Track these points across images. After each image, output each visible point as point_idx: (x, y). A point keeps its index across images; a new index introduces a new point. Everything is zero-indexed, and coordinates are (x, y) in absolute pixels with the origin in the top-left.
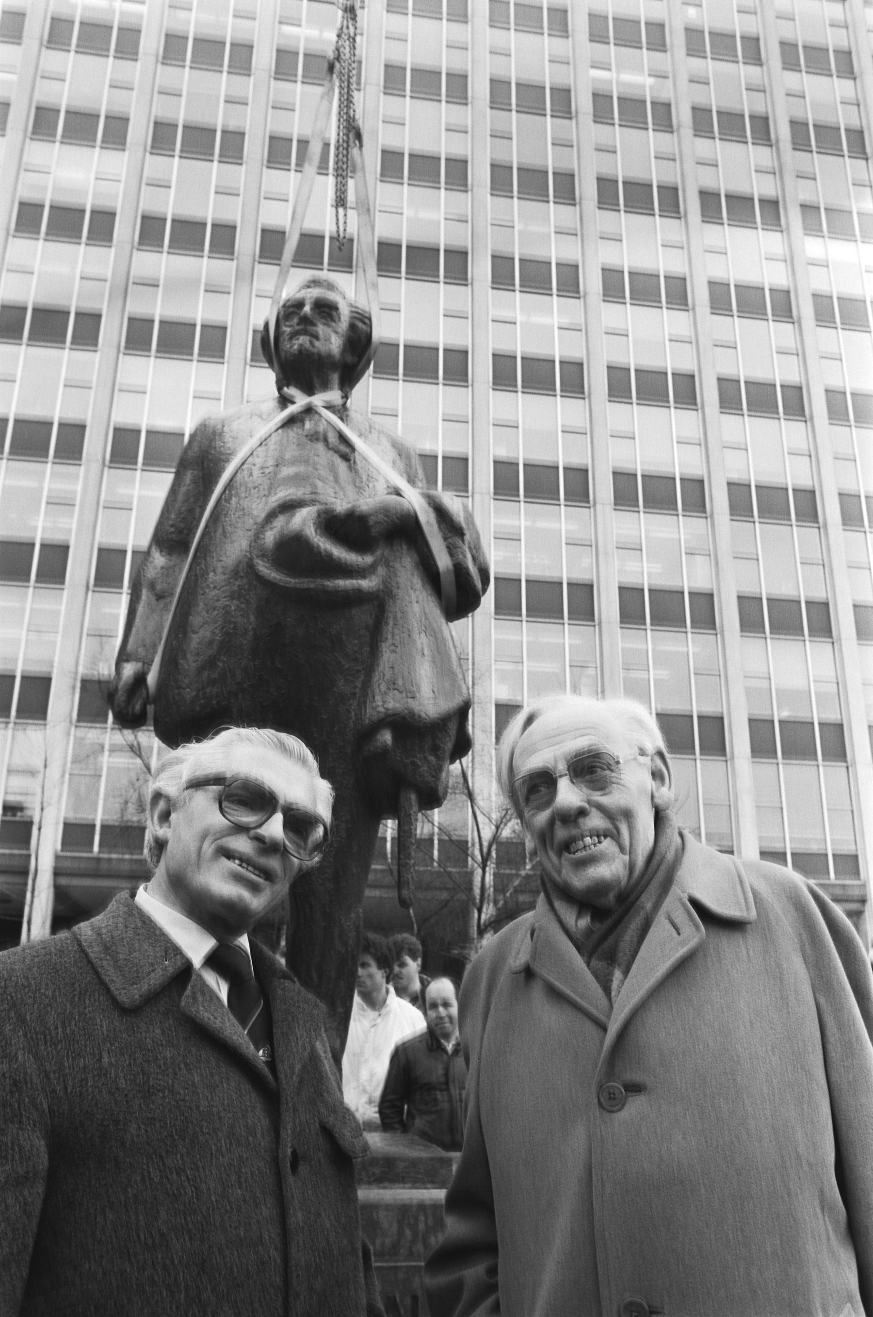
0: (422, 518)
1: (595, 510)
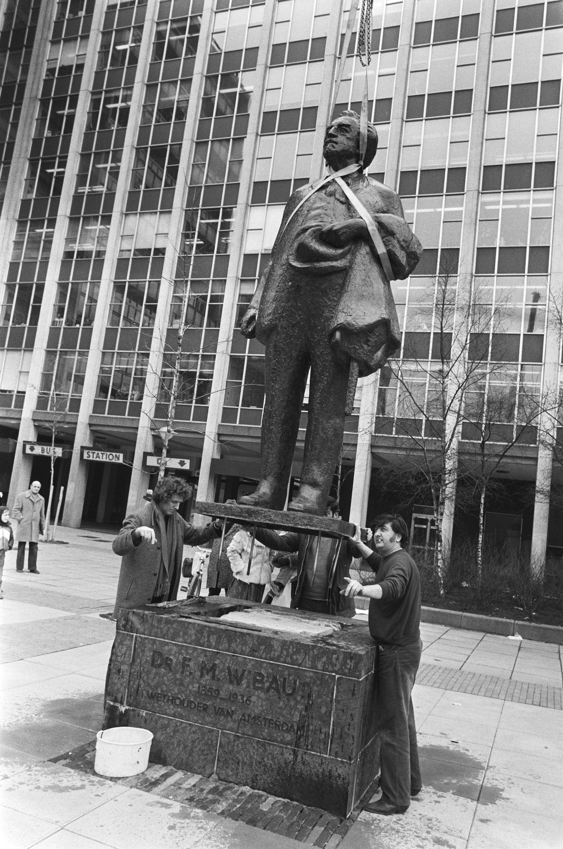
0: (370, 228)
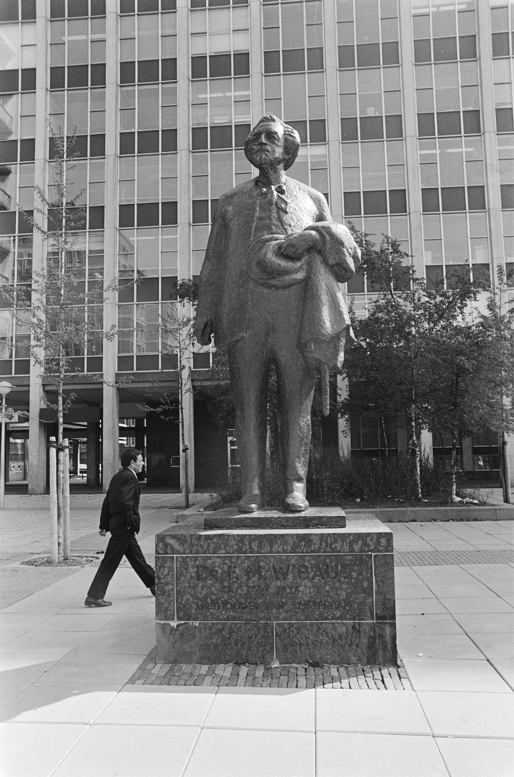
1: (410, 217)
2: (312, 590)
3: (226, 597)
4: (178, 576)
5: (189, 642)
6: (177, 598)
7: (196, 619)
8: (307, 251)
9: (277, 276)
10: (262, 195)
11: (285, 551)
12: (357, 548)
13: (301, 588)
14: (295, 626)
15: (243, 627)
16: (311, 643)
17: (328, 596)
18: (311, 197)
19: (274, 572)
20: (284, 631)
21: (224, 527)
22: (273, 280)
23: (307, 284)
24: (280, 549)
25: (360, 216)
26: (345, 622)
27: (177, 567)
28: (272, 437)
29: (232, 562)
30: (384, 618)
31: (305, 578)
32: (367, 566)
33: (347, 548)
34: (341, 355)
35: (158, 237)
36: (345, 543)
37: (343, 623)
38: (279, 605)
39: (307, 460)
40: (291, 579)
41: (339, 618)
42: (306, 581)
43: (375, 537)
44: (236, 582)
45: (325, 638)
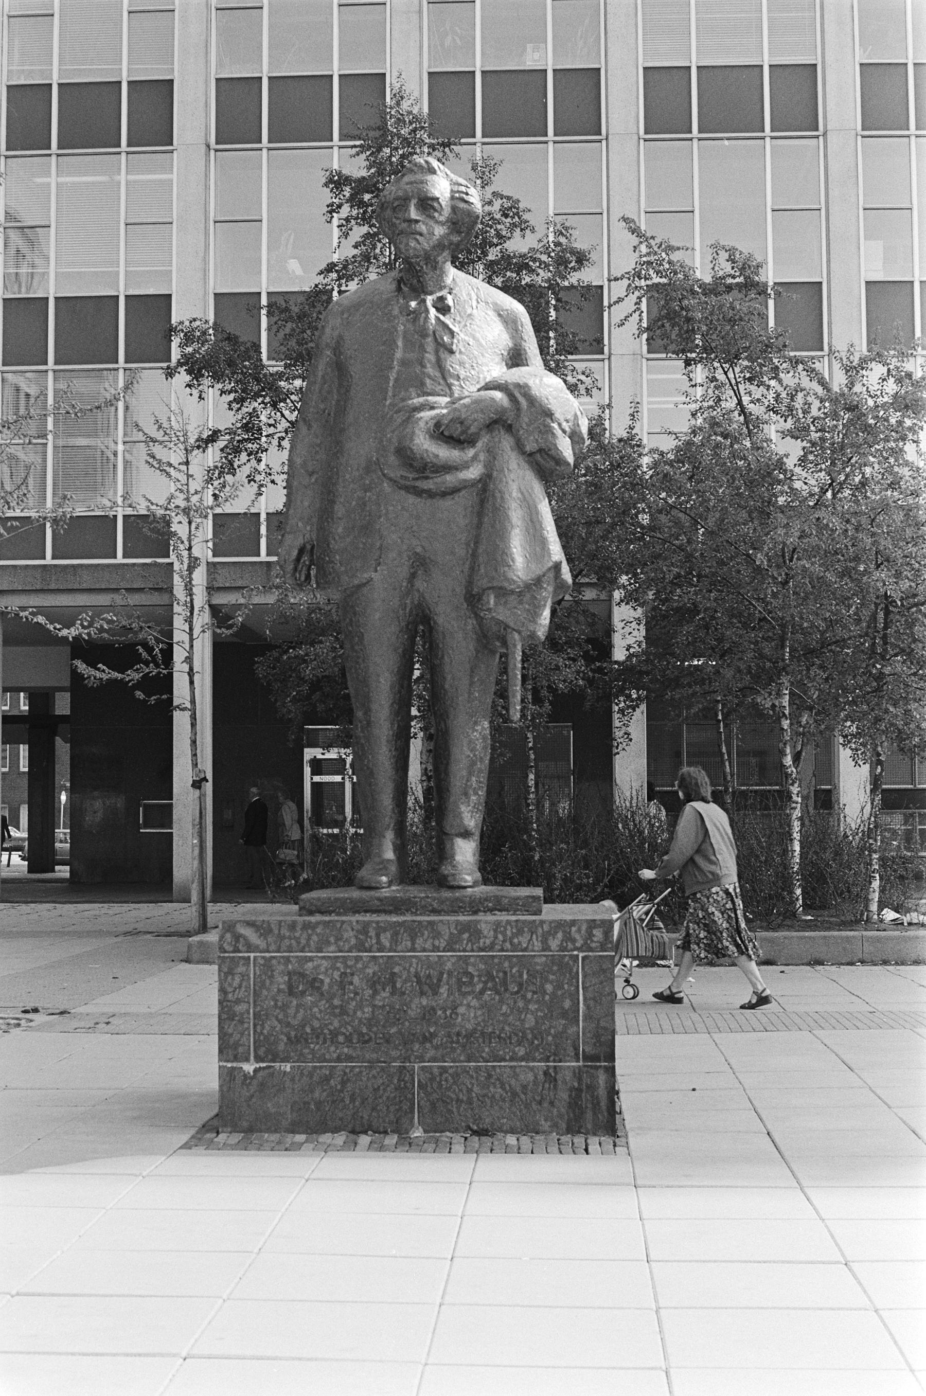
1: (825, 142)
2: (479, 1013)
3: (336, 1024)
4: (257, 988)
5: (274, 1097)
6: (255, 1025)
7: (285, 1060)
8: (488, 426)
9: (431, 475)
10: (408, 315)
11: (436, 949)
12: (554, 944)
13: (461, 1010)
14: (451, 1071)
15: (364, 1073)
16: (475, 1100)
17: (505, 1022)
18: (500, 315)
19: (417, 983)
20: (432, 1079)
21: (333, 912)
22: (425, 482)
23: (485, 490)
24: (428, 945)
25: (688, 136)
26: (531, 1064)
27: (255, 974)
28: (430, 751)
29: (347, 966)
30: (595, 1058)
31: (469, 993)
32: (570, 974)
33: (537, 945)
34: (544, 614)
35: (117, 178)
36: (534, 936)
37: (528, 1067)
38: (425, 1037)
39: (482, 800)
40: (445, 995)
41: (522, 1059)
42: (470, 998)
43: (584, 928)
44: (352, 999)
45: (500, 1090)
